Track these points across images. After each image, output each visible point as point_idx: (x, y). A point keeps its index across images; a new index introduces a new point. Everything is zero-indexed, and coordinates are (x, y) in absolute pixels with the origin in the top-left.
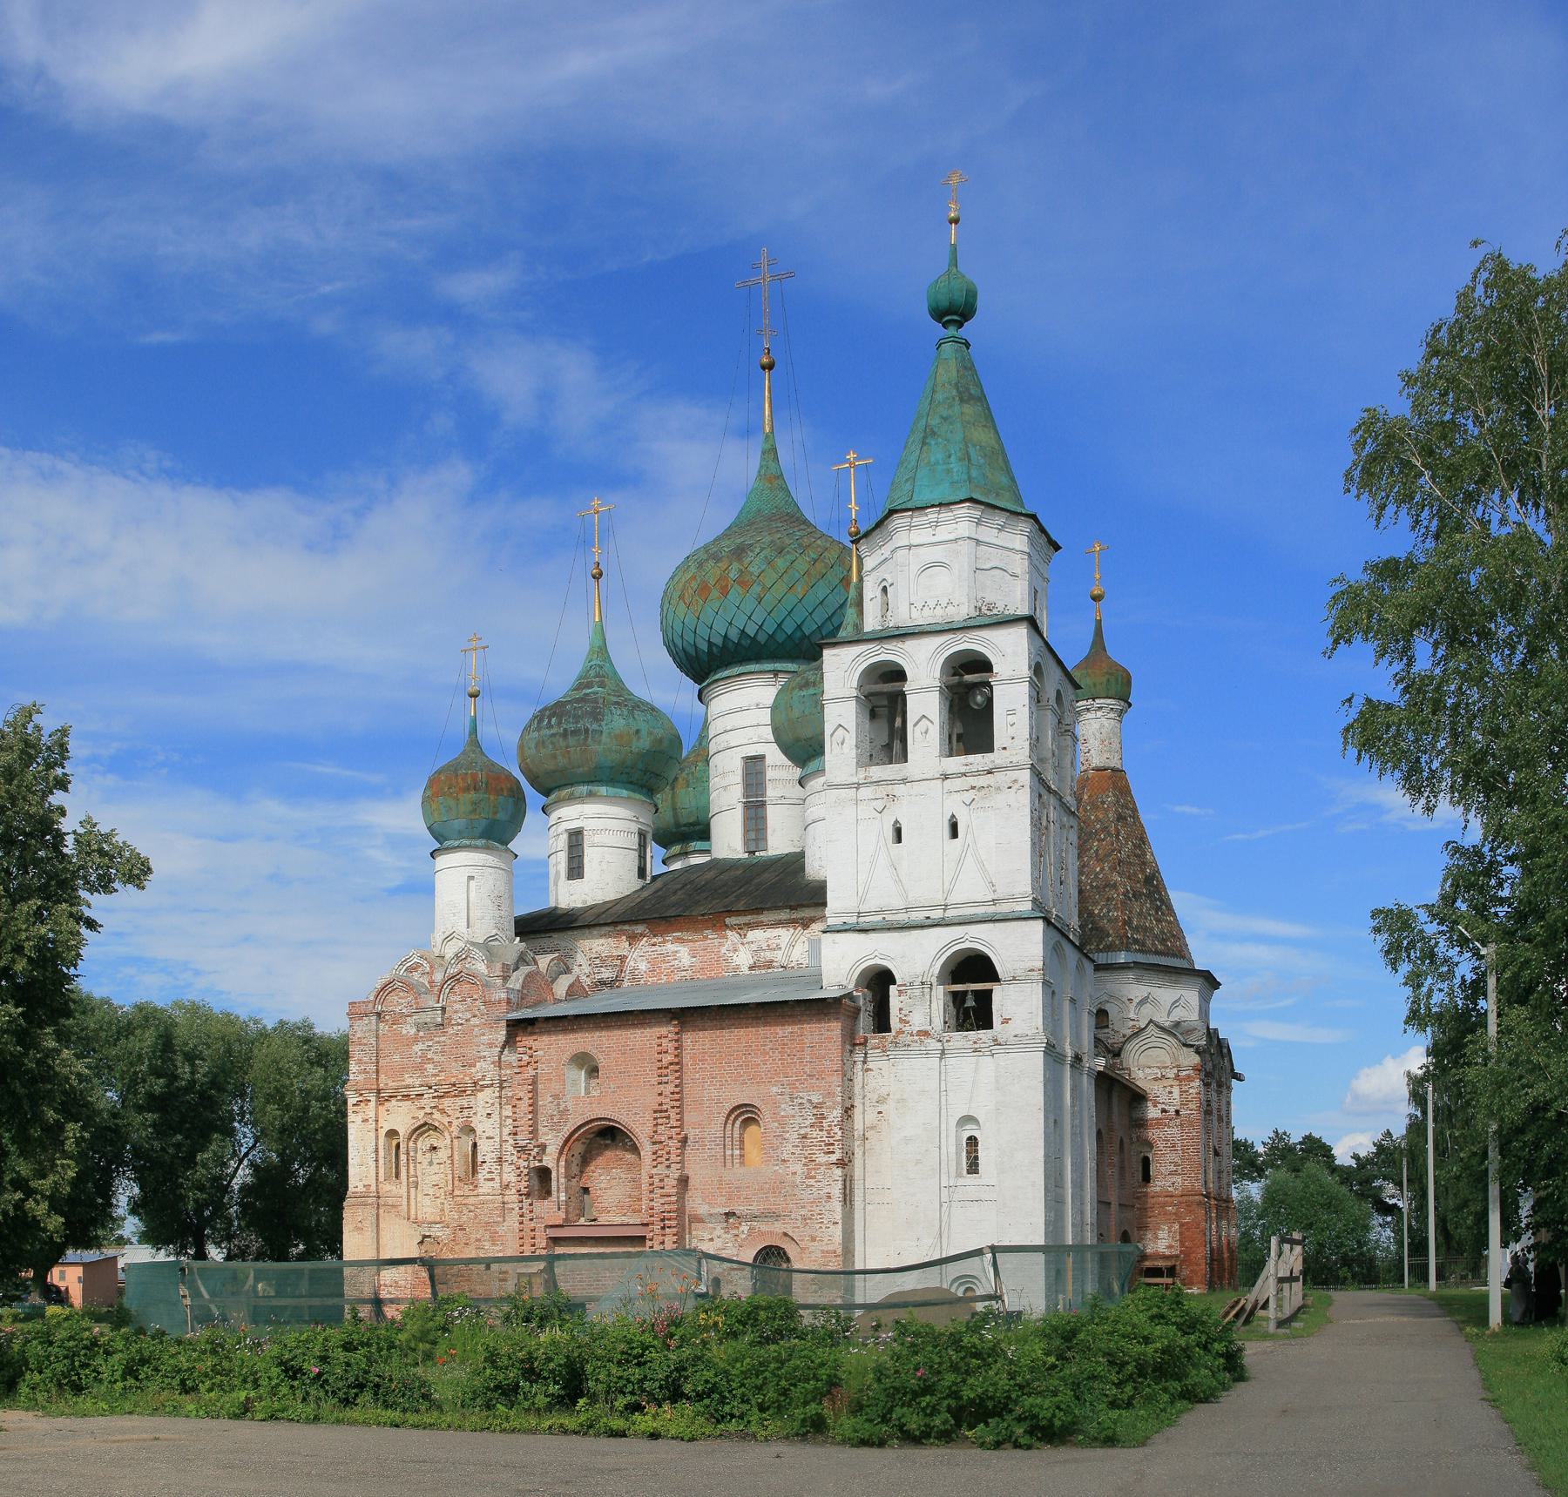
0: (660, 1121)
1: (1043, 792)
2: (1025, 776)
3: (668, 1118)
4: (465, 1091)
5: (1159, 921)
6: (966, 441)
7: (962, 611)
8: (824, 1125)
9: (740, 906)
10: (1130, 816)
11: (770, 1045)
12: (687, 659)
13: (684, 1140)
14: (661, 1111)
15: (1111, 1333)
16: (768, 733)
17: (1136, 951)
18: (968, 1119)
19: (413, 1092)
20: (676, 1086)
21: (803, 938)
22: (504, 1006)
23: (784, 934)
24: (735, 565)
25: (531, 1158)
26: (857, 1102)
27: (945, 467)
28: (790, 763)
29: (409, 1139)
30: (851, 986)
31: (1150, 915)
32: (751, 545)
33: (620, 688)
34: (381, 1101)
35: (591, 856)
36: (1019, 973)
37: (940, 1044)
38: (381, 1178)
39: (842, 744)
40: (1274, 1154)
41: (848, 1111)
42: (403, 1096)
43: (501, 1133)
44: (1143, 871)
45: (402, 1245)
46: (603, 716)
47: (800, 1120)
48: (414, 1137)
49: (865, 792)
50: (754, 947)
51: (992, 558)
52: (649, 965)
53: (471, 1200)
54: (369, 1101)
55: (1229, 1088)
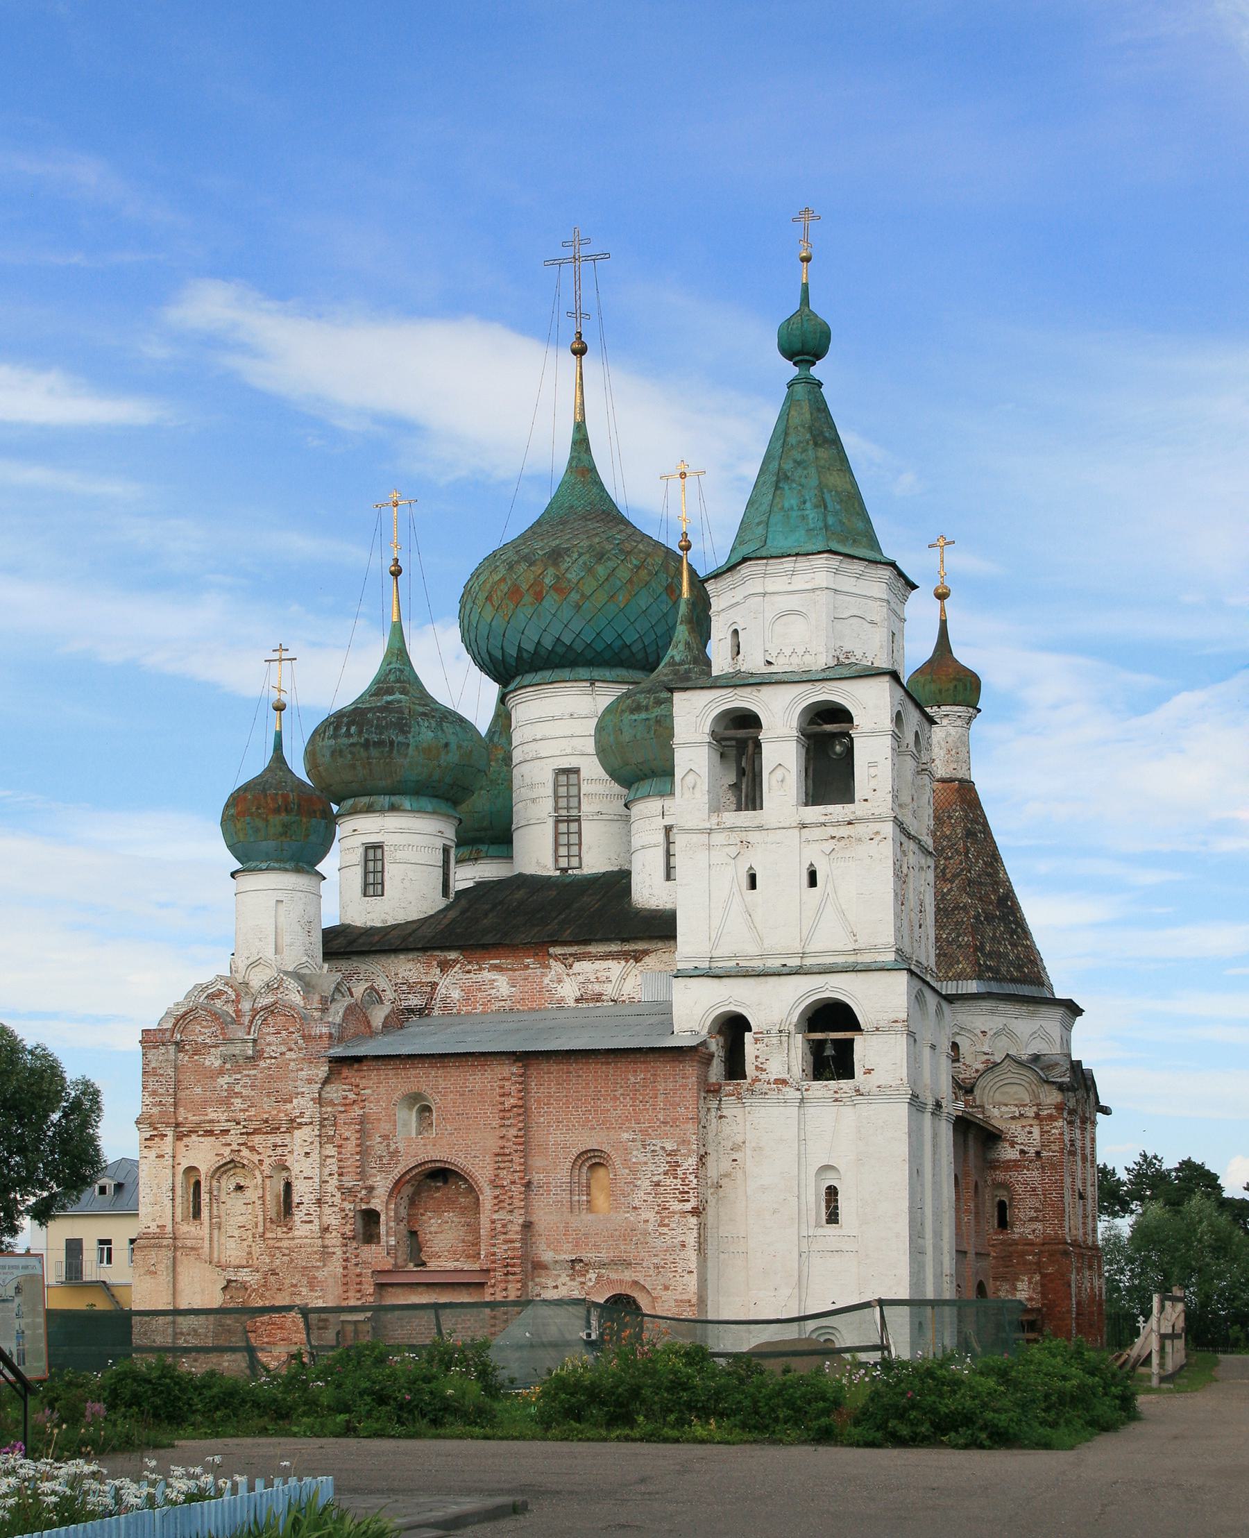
0: (502, 1165)
1: (904, 839)
2: (888, 828)
3: (511, 1161)
4: (278, 1129)
5: (1014, 945)
6: (821, 487)
7: (820, 660)
8: (679, 1172)
9: (566, 935)
10: (980, 832)
11: (621, 1091)
12: (491, 661)
13: (528, 1185)
14: (504, 1155)
15: (1037, 1372)
16: (590, 745)
17: (989, 979)
18: (828, 1168)
19: (217, 1129)
20: (520, 1130)
22: (326, 1041)
24: (551, 571)
25: (358, 1200)
27: (800, 513)
28: (607, 777)
29: (212, 1177)
30: (704, 1032)
31: (1004, 939)
32: (568, 549)
33: (425, 698)
34: (179, 1137)
35: (392, 873)
36: (882, 1024)
37: (799, 1093)
38: (178, 1219)
39: (693, 788)
40: (1142, 1183)
41: (702, 1158)
42: (205, 1131)
44: (995, 891)
45: (203, 1291)
46: (410, 728)
47: (653, 1167)
48: (218, 1175)
49: (718, 838)
50: (581, 978)
51: (851, 607)
52: (462, 994)
53: (285, 1244)
54: (166, 1135)
55: (1094, 1123)
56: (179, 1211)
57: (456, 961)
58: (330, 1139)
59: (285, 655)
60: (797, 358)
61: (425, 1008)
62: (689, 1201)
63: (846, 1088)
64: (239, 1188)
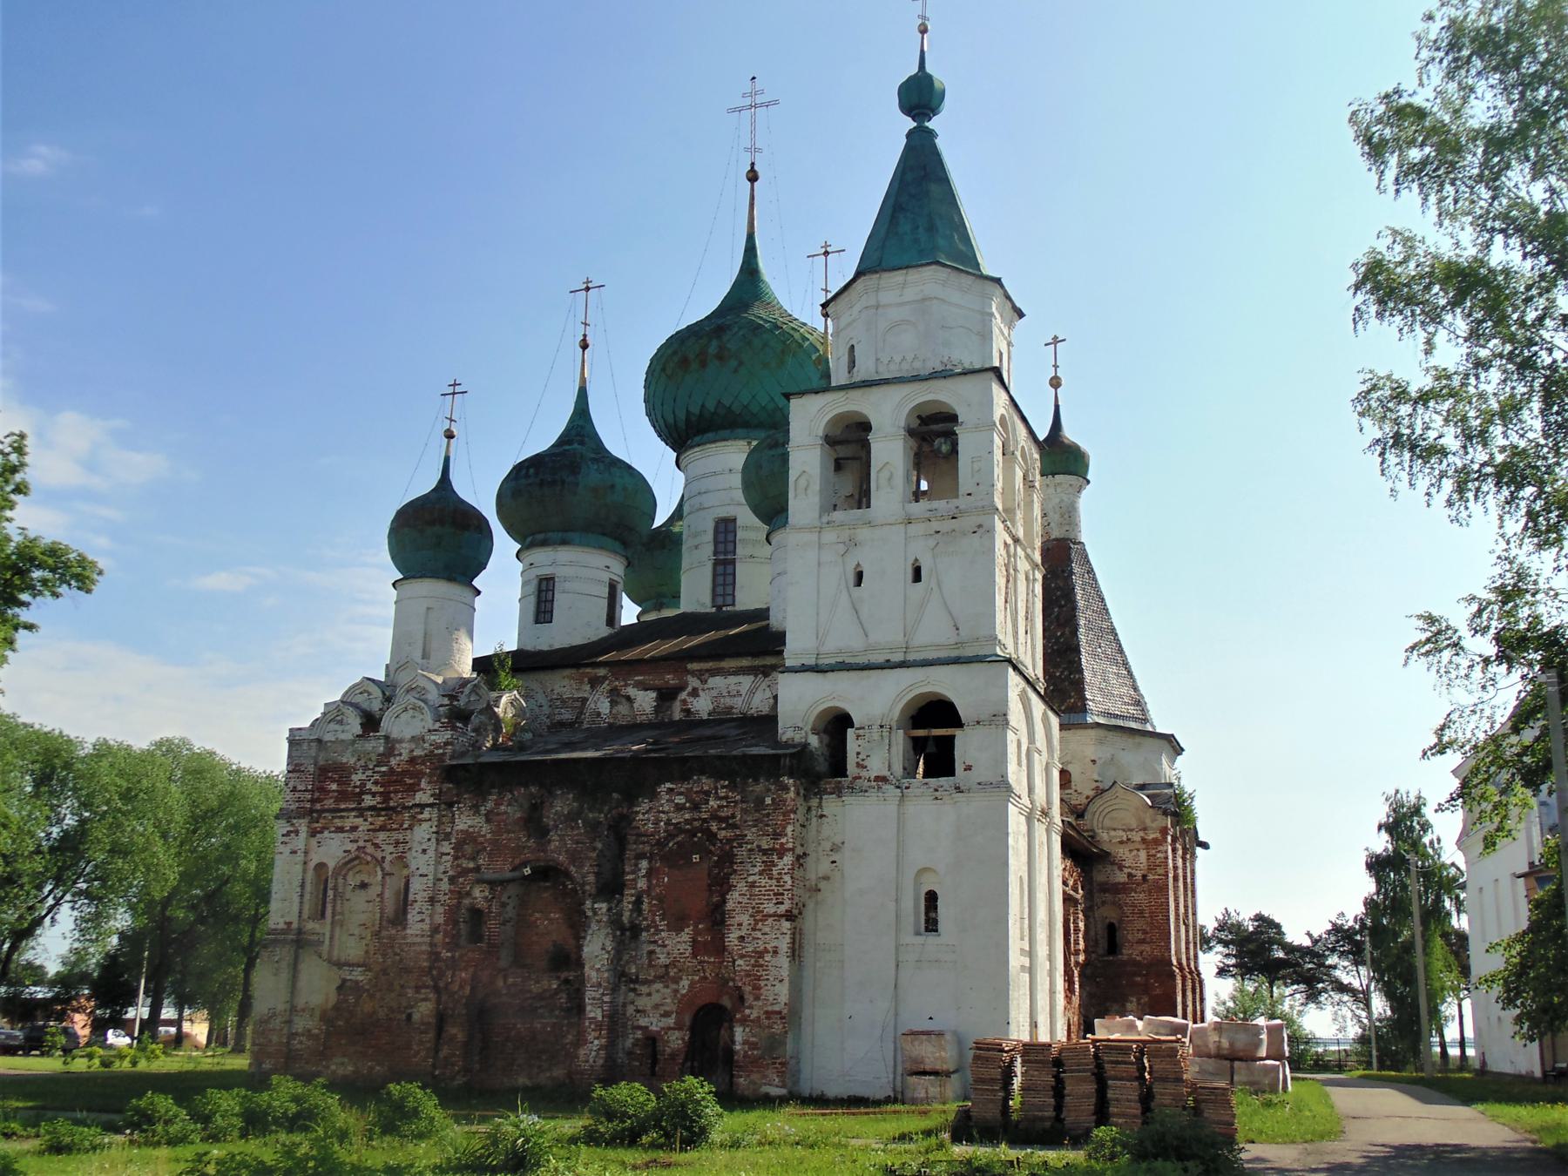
8: (774, 873)
12: (666, 426)
16: (739, 495)
21: (764, 685)
23: (746, 681)
26: (811, 849)
35: (561, 602)
36: (982, 717)
37: (899, 790)
38: (305, 916)
43: (436, 870)
50: (714, 693)
55: (1193, 855)
56: (306, 907)
57: (605, 678)
58: (447, 837)
59: (458, 389)
60: (914, 112)
61: (576, 722)
62: (783, 903)
63: (946, 786)
64: (364, 886)
